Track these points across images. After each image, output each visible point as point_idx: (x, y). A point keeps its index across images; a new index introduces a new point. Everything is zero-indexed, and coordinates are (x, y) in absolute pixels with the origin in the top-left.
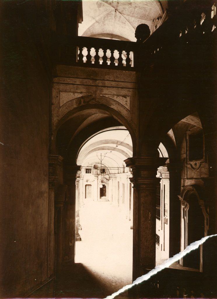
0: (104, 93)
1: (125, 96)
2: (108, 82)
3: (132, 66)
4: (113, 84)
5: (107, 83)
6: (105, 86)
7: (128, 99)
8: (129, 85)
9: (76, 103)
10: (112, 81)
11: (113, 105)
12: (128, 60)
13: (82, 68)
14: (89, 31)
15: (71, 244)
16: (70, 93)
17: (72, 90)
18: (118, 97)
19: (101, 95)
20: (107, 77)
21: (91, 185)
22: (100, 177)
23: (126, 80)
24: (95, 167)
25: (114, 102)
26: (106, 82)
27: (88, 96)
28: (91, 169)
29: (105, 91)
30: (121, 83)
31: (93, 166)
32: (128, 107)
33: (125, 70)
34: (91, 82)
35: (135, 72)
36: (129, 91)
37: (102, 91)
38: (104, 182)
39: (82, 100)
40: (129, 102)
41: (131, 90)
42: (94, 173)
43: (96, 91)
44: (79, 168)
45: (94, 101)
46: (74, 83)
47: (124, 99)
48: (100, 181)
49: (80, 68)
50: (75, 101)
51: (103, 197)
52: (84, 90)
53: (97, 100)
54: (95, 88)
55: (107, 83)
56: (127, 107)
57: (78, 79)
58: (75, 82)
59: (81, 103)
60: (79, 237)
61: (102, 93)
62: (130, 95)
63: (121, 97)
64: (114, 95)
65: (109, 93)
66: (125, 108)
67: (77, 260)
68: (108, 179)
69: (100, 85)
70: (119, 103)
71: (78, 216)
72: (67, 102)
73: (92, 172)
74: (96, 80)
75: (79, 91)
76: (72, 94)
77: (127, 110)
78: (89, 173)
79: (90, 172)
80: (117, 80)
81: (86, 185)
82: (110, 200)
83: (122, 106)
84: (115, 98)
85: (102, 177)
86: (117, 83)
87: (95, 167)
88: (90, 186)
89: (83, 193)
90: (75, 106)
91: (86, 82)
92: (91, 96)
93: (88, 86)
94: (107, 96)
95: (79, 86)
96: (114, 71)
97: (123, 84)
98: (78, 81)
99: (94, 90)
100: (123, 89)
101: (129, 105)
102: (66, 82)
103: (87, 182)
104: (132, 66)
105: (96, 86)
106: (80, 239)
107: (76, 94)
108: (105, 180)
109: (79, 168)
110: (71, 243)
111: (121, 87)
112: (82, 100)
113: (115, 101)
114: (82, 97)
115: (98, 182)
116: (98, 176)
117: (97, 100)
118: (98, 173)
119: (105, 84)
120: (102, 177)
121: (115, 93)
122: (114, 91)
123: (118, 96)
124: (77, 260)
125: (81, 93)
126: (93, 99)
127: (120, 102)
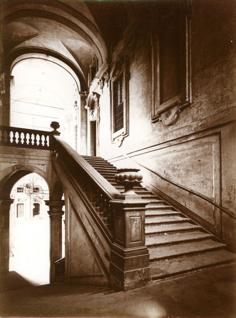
1: (43, 165)
3: (48, 146)
4: (36, 157)
6: (31, 159)
7: (45, 166)
8: (46, 158)
11: (36, 170)
12: (46, 142)
13: (15, 148)
16: (8, 163)
19: (28, 164)
20: (31, 154)
21: (23, 204)
22: (32, 195)
23: (44, 156)
24: (27, 186)
25: (36, 168)
26: (31, 156)
27: (19, 165)
28: (23, 188)
29: (31, 162)
30: (40, 157)
31: (25, 185)
32: (45, 171)
34: (21, 156)
36: (46, 161)
37: (28, 161)
38: (37, 200)
39: (15, 167)
40: (46, 168)
41: (47, 161)
42: (26, 191)
43: (24, 162)
46: (10, 157)
52: (16, 161)
54: (24, 160)
55: (32, 157)
56: (45, 171)
59: (15, 169)
60: (12, 253)
61: (29, 163)
63: (41, 165)
65: (33, 163)
66: (43, 172)
67: (11, 269)
73: (24, 191)
74: (25, 155)
75: (13, 162)
76: (9, 164)
79: (23, 191)
80: (38, 155)
81: (18, 205)
82: (43, 218)
83: (41, 170)
87: (27, 186)
88: (22, 205)
89: (14, 213)
91: (18, 157)
92: (21, 165)
93: (19, 159)
94: (32, 165)
95: (13, 159)
97: (42, 158)
98: (13, 156)
99: (23, 161)
101: (46, 170)
102: (5, 157)
103: (19, 201)
104: (48, 146)
105: (25, 159)
107: (11, 164)
108: (38, 199)
110: (6, 256)
111: (41, 159)
112: (15, 167)
113: (37, 168)
114: (15, 166)
115: (31, 201)
117: (25, 167)
118: (31, 192)
121: (37, 163)
122: (36, 162)
123: (39, 165)
124: (11, 269)
125: (15, 163)
126: (23, 166)
127: (40, 168)
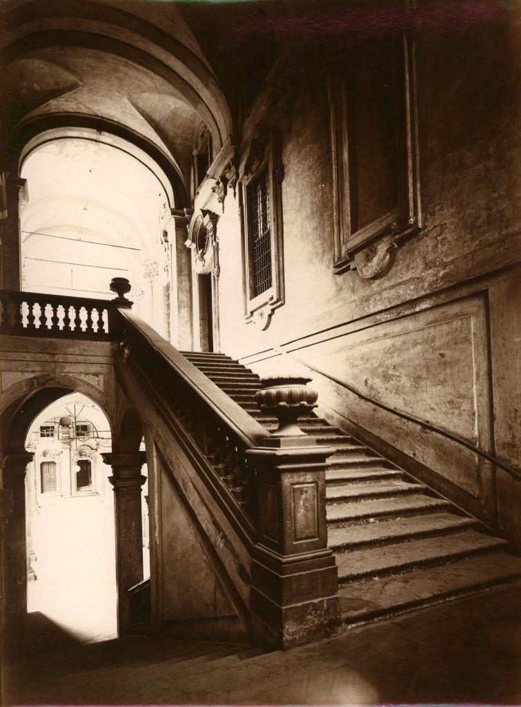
0: (66, 371)
1: (96, 375)
2: (73, 356)
3: (107, 331)
4: (80, 358)
5: (70, 358)
7: (101, 378)
9: (27, 385)
10: (78, 355)
12: (101, 323)
14: (50, 479)
15: (20, 583)
17: (20, 368)
18: (87, 376)
19: (63, 374)
20: (70, 350)
21: (54, 463)
23: (98, 354)
28: (53, 427)
29: (68, 368)
30: (90, 358)
32: (101, 388)
33: (96, 340)
34: (47, 357)
35: (109, 343)
37: (63, 367)
39: (35, 382)
41: (104, 366)
42: (61, 435)
43: (55, 369)
44: (29, 457)
45: (52, 382)
46: (22, 359)
47: (96, 377)
48: (74, 452)
49: (31, 338)
50: (24, 383)
51: (84, 489)
52: (37, 368)
53: (57, 380)
55: (70, 358)
57: (28, 354)
58: (24, 358)
61: (64, 371)
62: (103, 372)
64: (81, 373)
66: (97, 389)
67: (31, 609)
68: (96, 448)
69: (60, 361)
70: (88, 384)
71: (29, 534)
72: (13, 385)
73: (56, 435)
75: (30, 370)
76: (20, 374)
77: (100, 392)
78: (48, 435)
79: (52, 435)
80: (85, 354)
81: (42, 464)
82: (100, 493)
84: (82, 377)
85: (82, 443)
86: (84, 357)
90: (25, 390)
92: (47, 375)
94: (71, 375)
96: (80, 341)
98: (28, 357)
100: (94, 365)
101: (102, 385)
103: (45, 456)
104: (107, 331)
105: (55, 362)
106: (36, 578)
107: (26, 374)
108: (88, 451)
109: (29, 457)
112: (35, 382)
113: (82, 381)
114: (35, 378)
116: (70, 443)
117: (57, 380)
119: (67, 359)
120: (82, 443)
121: (83, 370)
122: (81, 368)
123: (86, 374)
124: (31, 609)
125: (34, 372)
126: (51, 379)
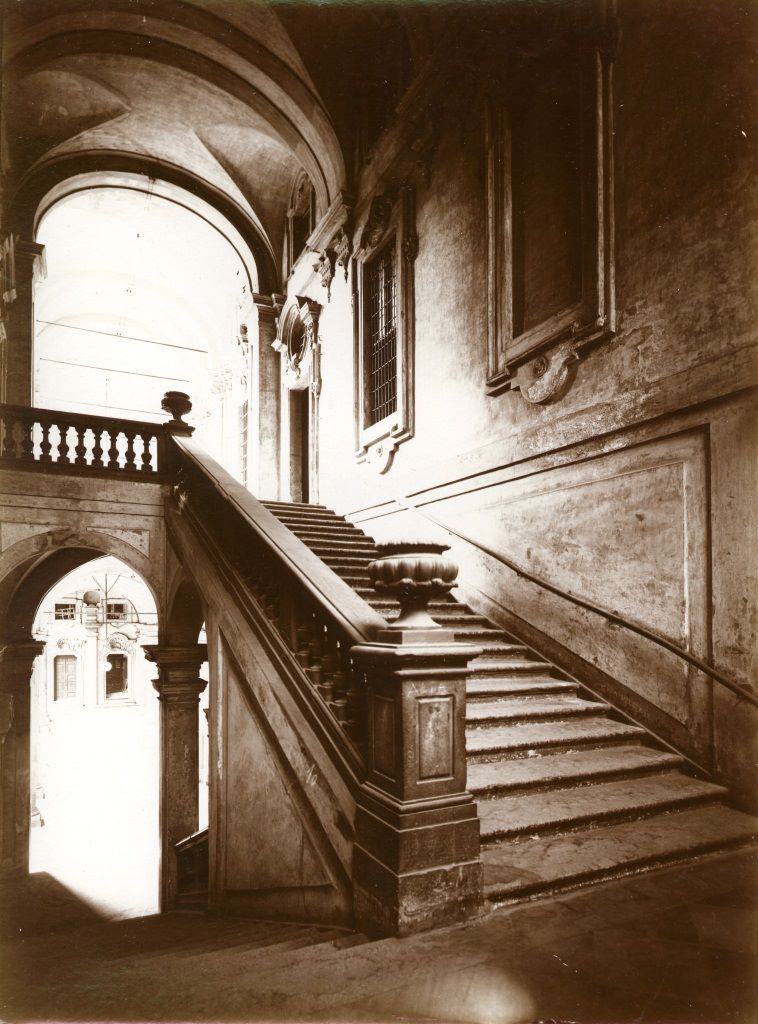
1: (138, 531)
3: (155, 469)
4: (115, 507)
6: (98, 512)
7: (145, 536)
8: (148, 510)
11: (115, 548)
12: (146, 457)
13: (49, 476)
16: (24, 525)
19: (90, 529)
20: (101, 495)
21: (73, 657)
22: (102, 629)
23: (141, 501)
24: (88, 600)
25: (116, 543)
26: (100, 503)
27: (61, 532)
28: (74, 606)
29: (98, 520)
30: (130, 506)
31: (81, 596)
32: (145, 551)
34: (68, 503)
36: (147, 520)
37: (90, 520)
38: (118, 645)
39: (50, 539)
40: (146, 542)
41: (150, 518)
42: (85, 617)
43: (78, 521)
46: (32, 505)
52: (53, 520)
54: (76, 514)
55: (101, 506)
56: (143, 552)
59: (47, 544)
60: (38, 816)
61: (92, 525)
63: (131, 533)
65: (107, 525)
66: (138, 552)
67: (35, 866)
73: (77, 617)
74: (79, 500)
75: (42, 521)
76: (27, 527)
79: (72, 616)
80: (122, 500)
81: (56, 659)
82: (138, 703)
83: (133, 549)
87: (88, 600)
88: (69, 662)
89: (46, 685)
91: (58, 504)
92: (67, 530)
93: (62, 512)
94: (101, 531)
95: (43, 511)
97: (134, 509)
98: (40, 502)
99: (75, 519)
101: (146, 547)
102: (15, 504)
103: (60, 647)
104: (155, 469)
105: (79, 511)
107: (36, 527)
108: (123, 641)
110: (21, 825)
111: (131, 512)
112: (50, 539)
113: (118, 539)
114: (49, 533)
115: (101, 646)
117: (80, 538)
118: (100, 619)
121: (119, 525)
122: (117, 521)
123: (124, 530)
124: (35, 866)
125: (47, 524)
126: (73, 536)
127: (128, 541)
